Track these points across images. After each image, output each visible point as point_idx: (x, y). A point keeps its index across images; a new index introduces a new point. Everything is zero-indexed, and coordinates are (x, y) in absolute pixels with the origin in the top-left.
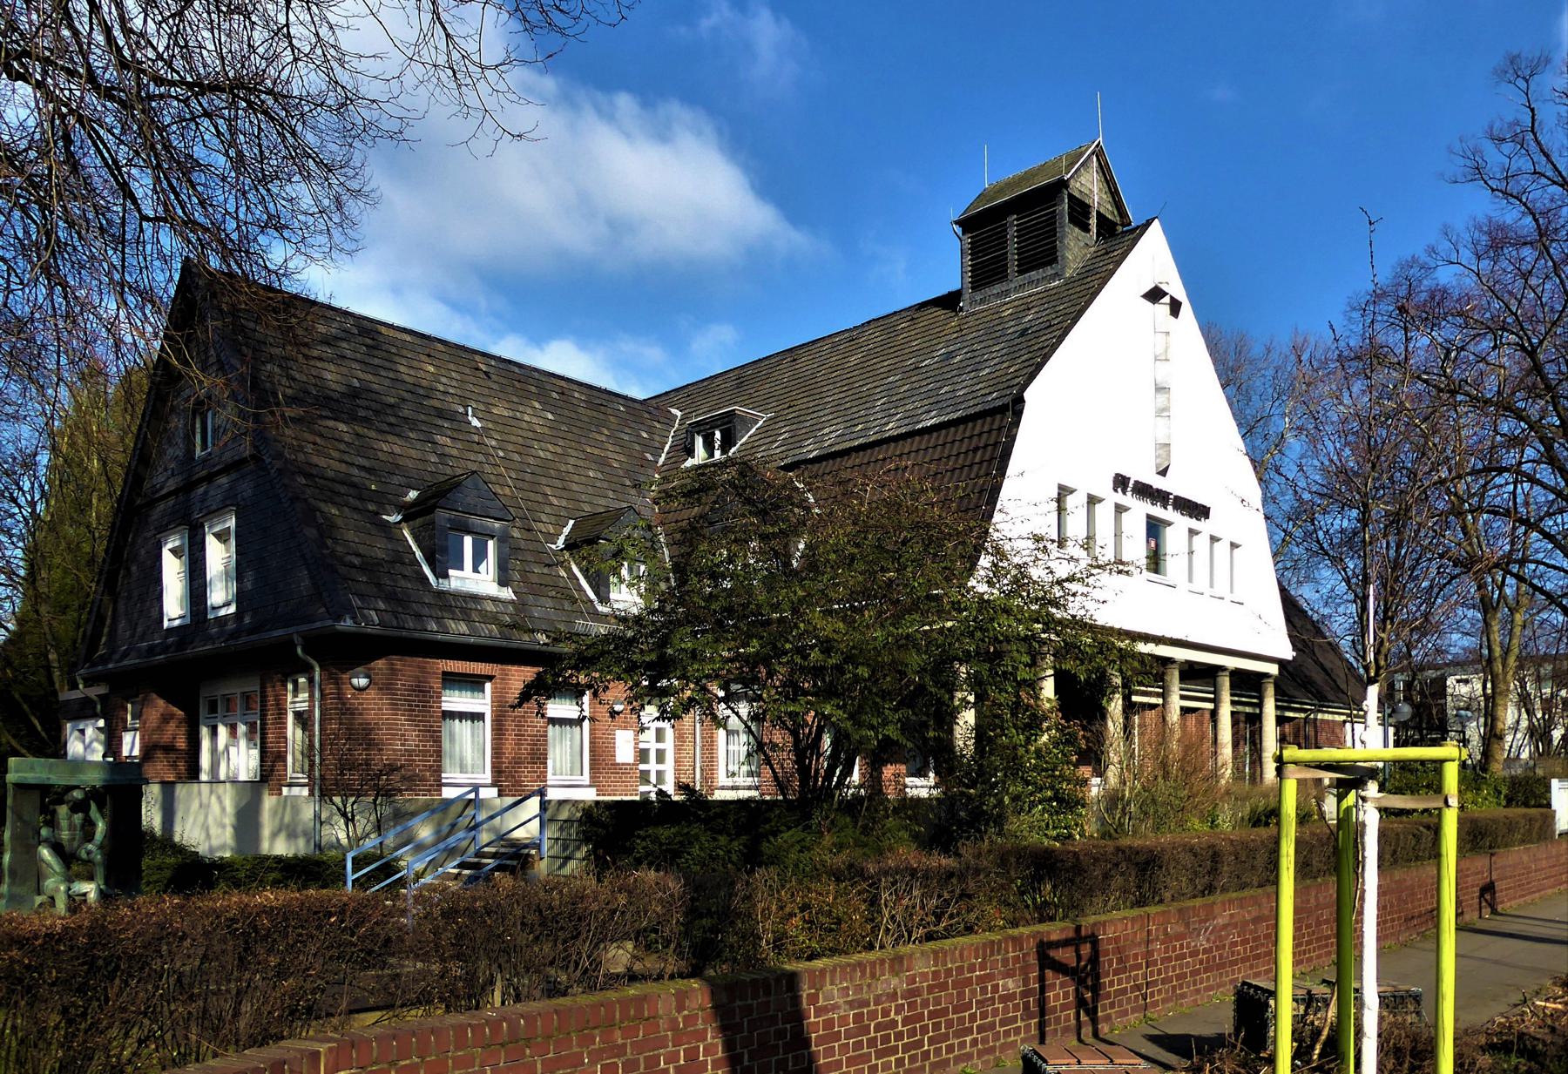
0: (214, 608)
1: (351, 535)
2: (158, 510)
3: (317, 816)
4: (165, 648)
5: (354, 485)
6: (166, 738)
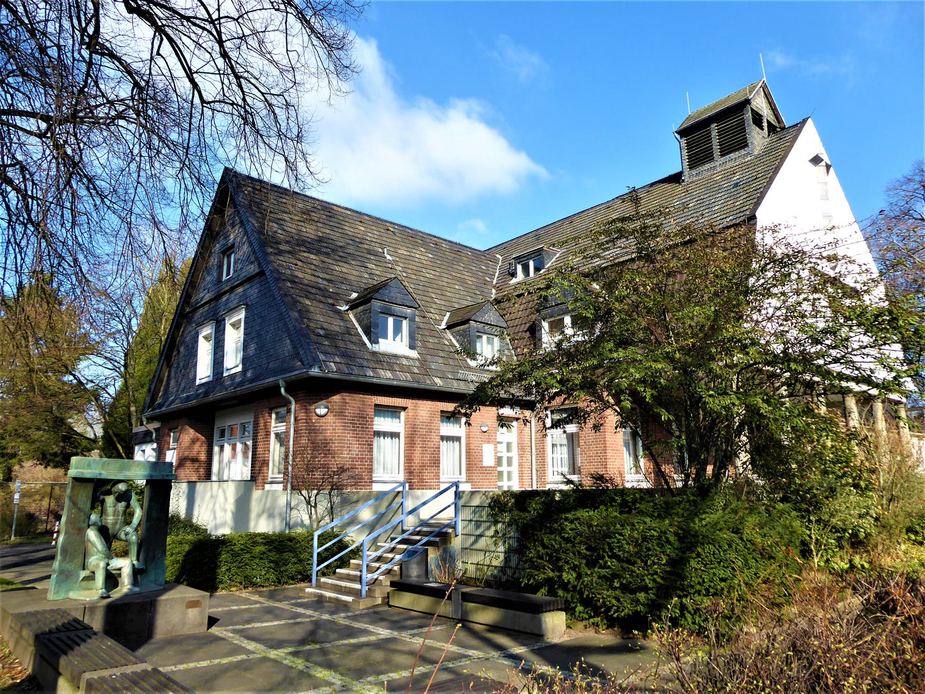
0: (227, 370)
1: (318, 317)
2: (198, 313)
3: (288, 504)
4: (197, 396)
5: (319, 289)
6: (193, 454)
